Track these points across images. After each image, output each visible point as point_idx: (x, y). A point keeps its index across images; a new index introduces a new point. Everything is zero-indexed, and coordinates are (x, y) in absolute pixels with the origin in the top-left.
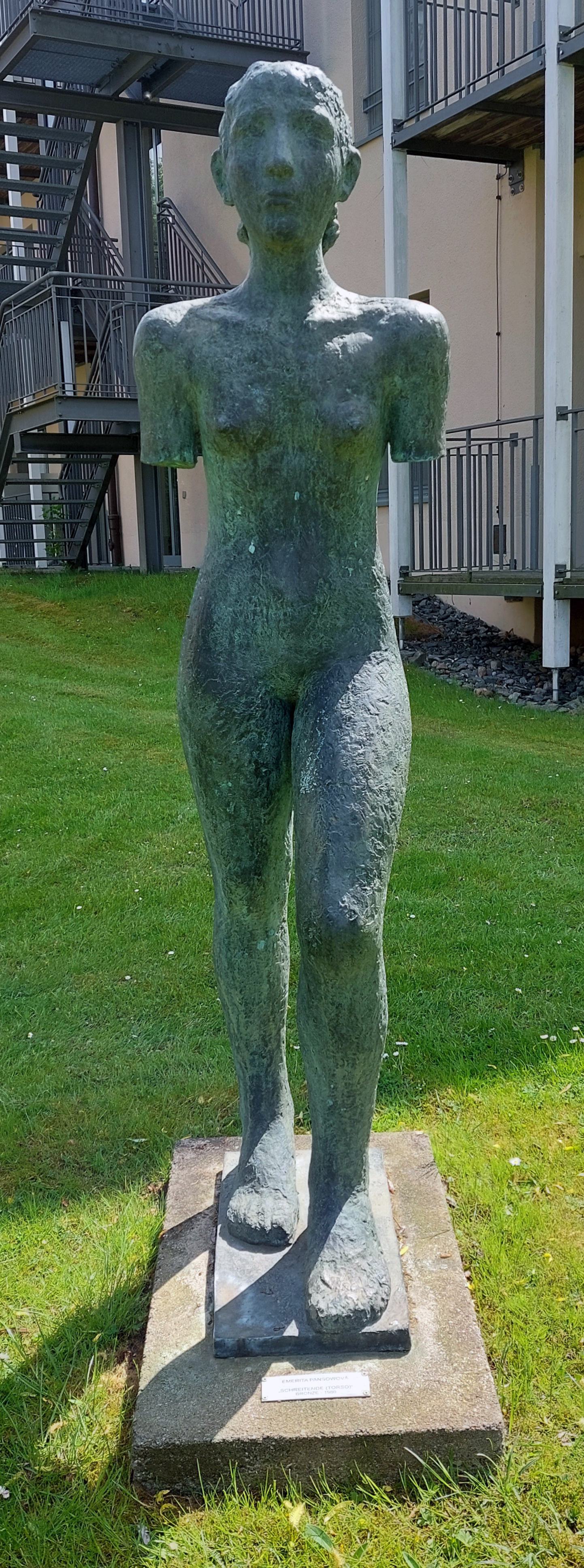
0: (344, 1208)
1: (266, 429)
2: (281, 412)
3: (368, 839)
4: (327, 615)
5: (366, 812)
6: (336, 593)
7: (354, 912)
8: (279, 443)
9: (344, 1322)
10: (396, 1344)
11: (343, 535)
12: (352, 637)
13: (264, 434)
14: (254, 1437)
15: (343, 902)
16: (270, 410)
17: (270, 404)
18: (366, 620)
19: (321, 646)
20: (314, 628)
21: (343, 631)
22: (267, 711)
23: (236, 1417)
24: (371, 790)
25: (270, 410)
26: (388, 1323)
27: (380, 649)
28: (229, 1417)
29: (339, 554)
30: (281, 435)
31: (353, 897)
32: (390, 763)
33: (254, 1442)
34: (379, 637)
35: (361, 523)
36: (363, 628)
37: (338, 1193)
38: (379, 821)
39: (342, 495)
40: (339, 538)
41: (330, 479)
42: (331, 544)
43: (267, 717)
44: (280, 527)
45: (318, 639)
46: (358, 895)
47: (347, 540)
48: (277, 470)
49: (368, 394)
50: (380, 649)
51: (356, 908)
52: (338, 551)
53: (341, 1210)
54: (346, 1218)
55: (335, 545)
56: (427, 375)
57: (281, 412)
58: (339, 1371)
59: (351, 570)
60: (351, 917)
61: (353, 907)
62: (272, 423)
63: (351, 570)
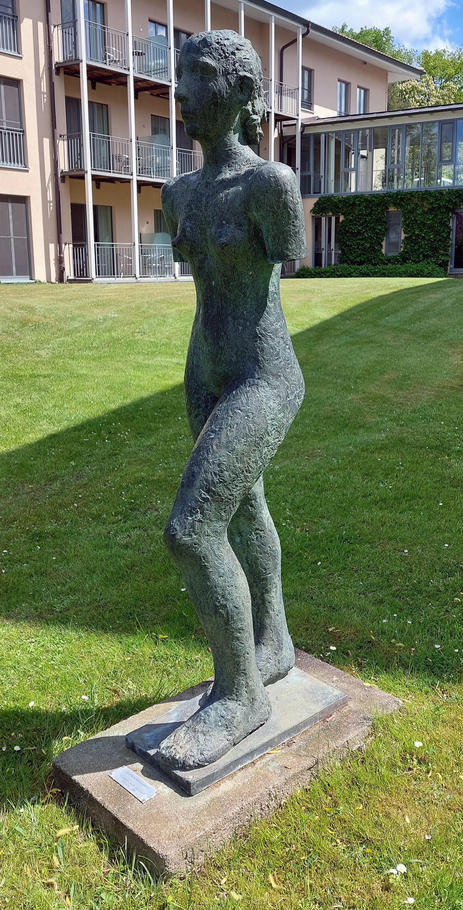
0: (215, 704)
1: (192, 245)
2: (199, 236)
3: (197, 489)
4: (226, 353)
5: (200, 473)
6: (230, 341)
7: (176, 529)
8: (201, 253)
9: (166, 760)
10: (184, 789)
11: (236, 307)
12: (239, 368)
13: (191, 248)
14: (84, 787)
15: (173, 522)
16: (193, 234)
17: (193, 231)
18: (248, 359)
19: (224, 371)
20: (220, 361)
21: (235, 363)
22: (209, 404)
23: (92, 774)
24: (208, 462)
25: (193, 234)
26: (189, 776)
27: (253, 377)
28: (90, 772)
29: (234, 318)
30: (201, 248)
31: (179, 521)
32: (227, 447)
33: (83, 788)
34: (255, 370)
35: (249, 300)
36: (246, 364)
37: (216, 694)
38: (207, 480)
39: (232, 283)
40: (234, 308)
41: (223, 274)
42: (229, 312)
43: (209, 408)
44: (208, 300)
45: (223, 367)
46: (181, 521)
47: (239, 310)
48: (202, 268)
49: (236, 224)
50: (253, 377)
51: (178, 528)
52: (234, 316)
53: (212, 703)
54: (211, 710)
55: (232, 313)
56: (267, 210)
57: (199, 236)
58: (151, 784)
59: (240, 328)
60: (173, 532)
61: (176, 527)
62: (194, 241)
63: (240, 328)
